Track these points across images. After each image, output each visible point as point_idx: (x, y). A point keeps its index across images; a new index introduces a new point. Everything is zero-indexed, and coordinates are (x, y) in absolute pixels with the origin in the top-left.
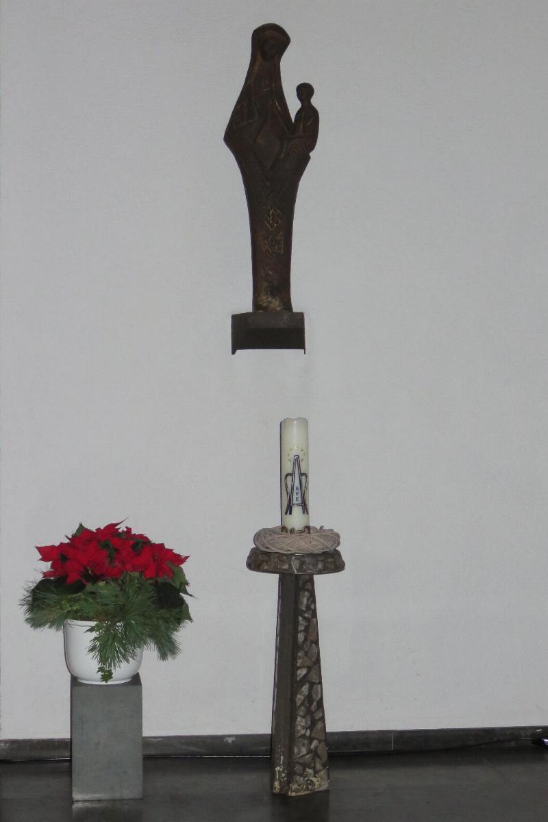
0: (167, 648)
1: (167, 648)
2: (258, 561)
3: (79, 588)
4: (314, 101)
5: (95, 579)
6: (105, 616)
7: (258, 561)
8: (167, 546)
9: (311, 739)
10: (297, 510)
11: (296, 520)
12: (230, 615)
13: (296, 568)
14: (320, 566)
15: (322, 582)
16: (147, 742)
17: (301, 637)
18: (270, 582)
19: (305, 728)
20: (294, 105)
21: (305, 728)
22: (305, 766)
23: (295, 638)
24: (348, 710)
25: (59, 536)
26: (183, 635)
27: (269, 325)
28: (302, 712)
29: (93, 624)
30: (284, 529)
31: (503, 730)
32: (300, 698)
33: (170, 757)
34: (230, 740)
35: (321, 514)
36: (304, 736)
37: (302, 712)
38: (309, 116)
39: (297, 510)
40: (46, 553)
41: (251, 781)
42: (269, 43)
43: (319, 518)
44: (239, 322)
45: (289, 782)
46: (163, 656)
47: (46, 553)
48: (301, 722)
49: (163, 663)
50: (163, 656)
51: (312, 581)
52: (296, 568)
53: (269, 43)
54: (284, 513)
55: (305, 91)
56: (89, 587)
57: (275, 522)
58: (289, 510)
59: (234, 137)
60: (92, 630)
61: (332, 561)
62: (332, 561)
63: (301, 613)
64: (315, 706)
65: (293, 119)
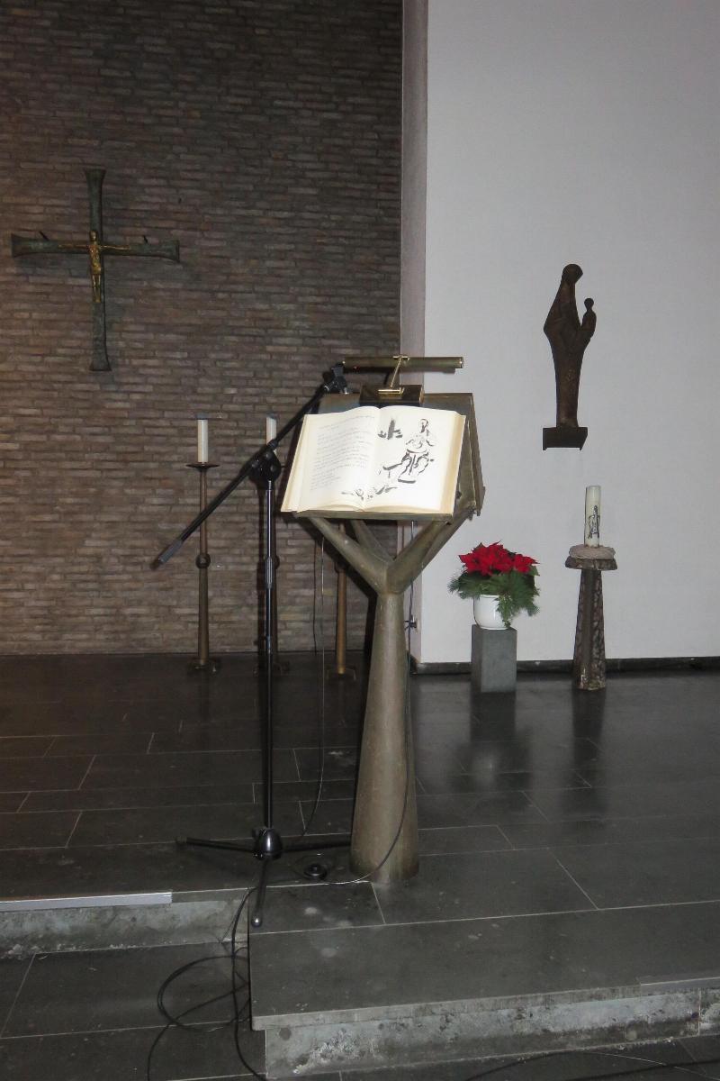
0: (532, 610)
1: (532, 610)
2: (571, 563)
3: (488, 577)
4: (594, 308)
5: (497, 571)
6: (503, 591)
7: (571, 563)
8: (524, 555)
9: (599, 659)
10: (594, 536)
11: (592, 542)
12: (558, 589)
13: (592, 570)
14: (609, 566)
15: (606, 575)
16: (606, 661)
17: (596, 605)
18: (576, 574)
19: (597, 654)
20: (581, 311)
21: (597, 654)
22: (596, 674)
23: (593, 606)
24: (617, 646)
25: (468, 550)
26: (537, 600)
27: (566, 434)
28: (595, 645)
29: (497, 597)
30: (586, 546)
31: (674, 658)
32: (595, 637)
33: (530, 671)
34: (537, 663)
35: (608, 539)
36: (596, 659)
37: (595, 645)
38: (591, 318)
39: (594, 536)
40: (463, 558)
41: (564, 685)
42: (572, 274)
43: (605, 541)
44: (547, 432)
45: (588, 683)
46: (530, 614)
47: (463, 558)
48: (595, 651)
49: (530, 618)
50: (530, 614)
51: (600, 574)
52: (592, 570)
53: (572, 274)
54: (587, 536)
55: (589, 303)
56: (494, 576)
57: (580, 542)
58: (590, 536)
59: (548, 328)
60: (497, 599)
61: (612, 565)
62: (612, 565)
63: (596, 591)
64: (600, 643)
65: (581, 321)
